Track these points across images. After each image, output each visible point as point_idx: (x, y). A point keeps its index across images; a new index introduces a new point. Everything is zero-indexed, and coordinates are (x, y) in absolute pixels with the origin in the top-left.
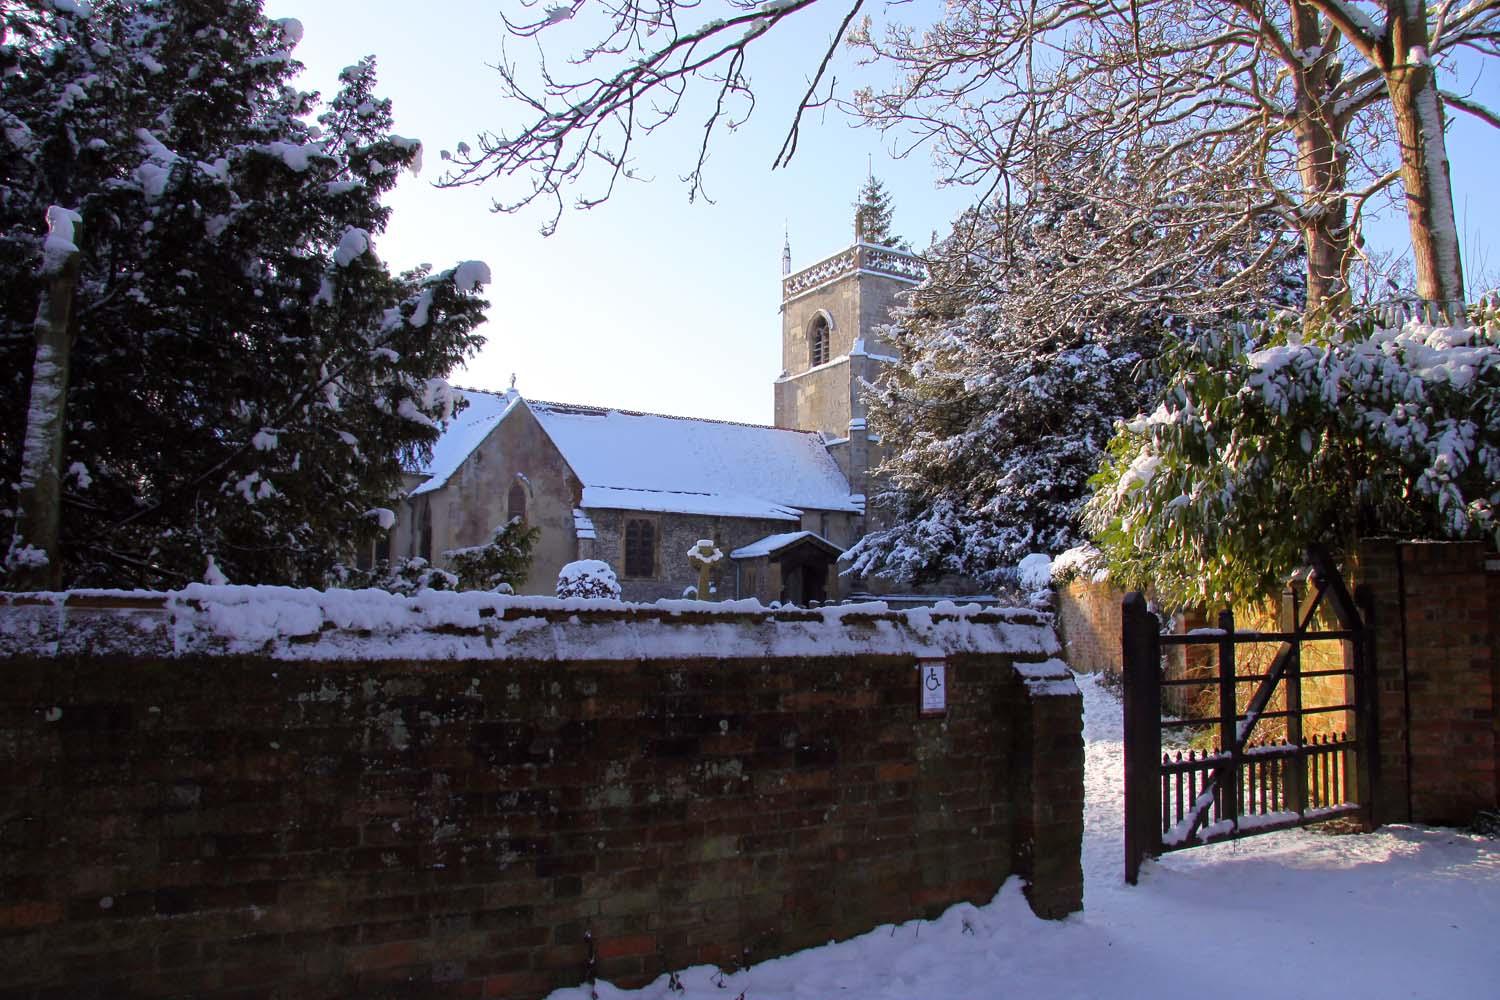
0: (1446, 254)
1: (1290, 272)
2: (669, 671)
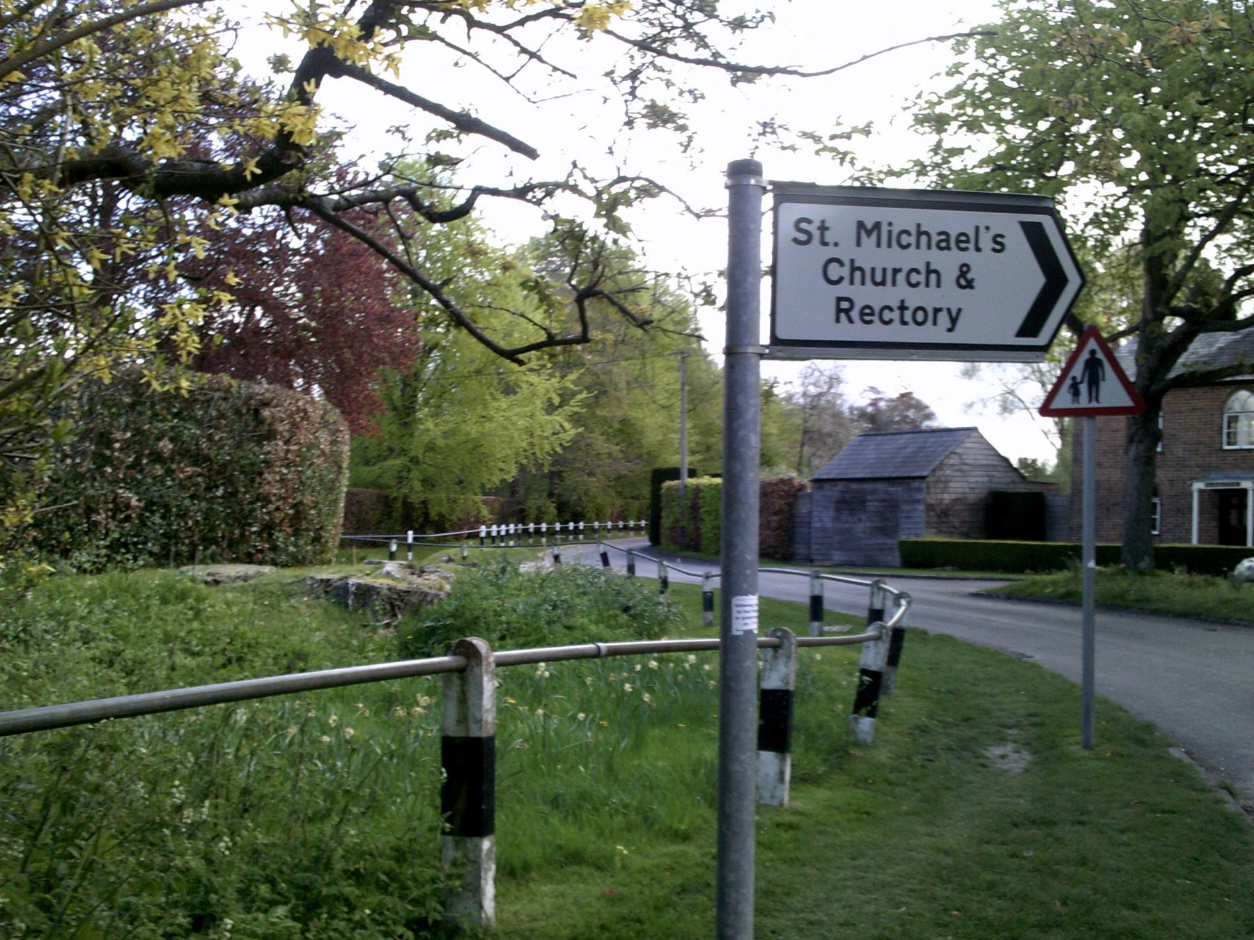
0: (1028, 354)
1: (850, 891)
2: (1170, 745)
